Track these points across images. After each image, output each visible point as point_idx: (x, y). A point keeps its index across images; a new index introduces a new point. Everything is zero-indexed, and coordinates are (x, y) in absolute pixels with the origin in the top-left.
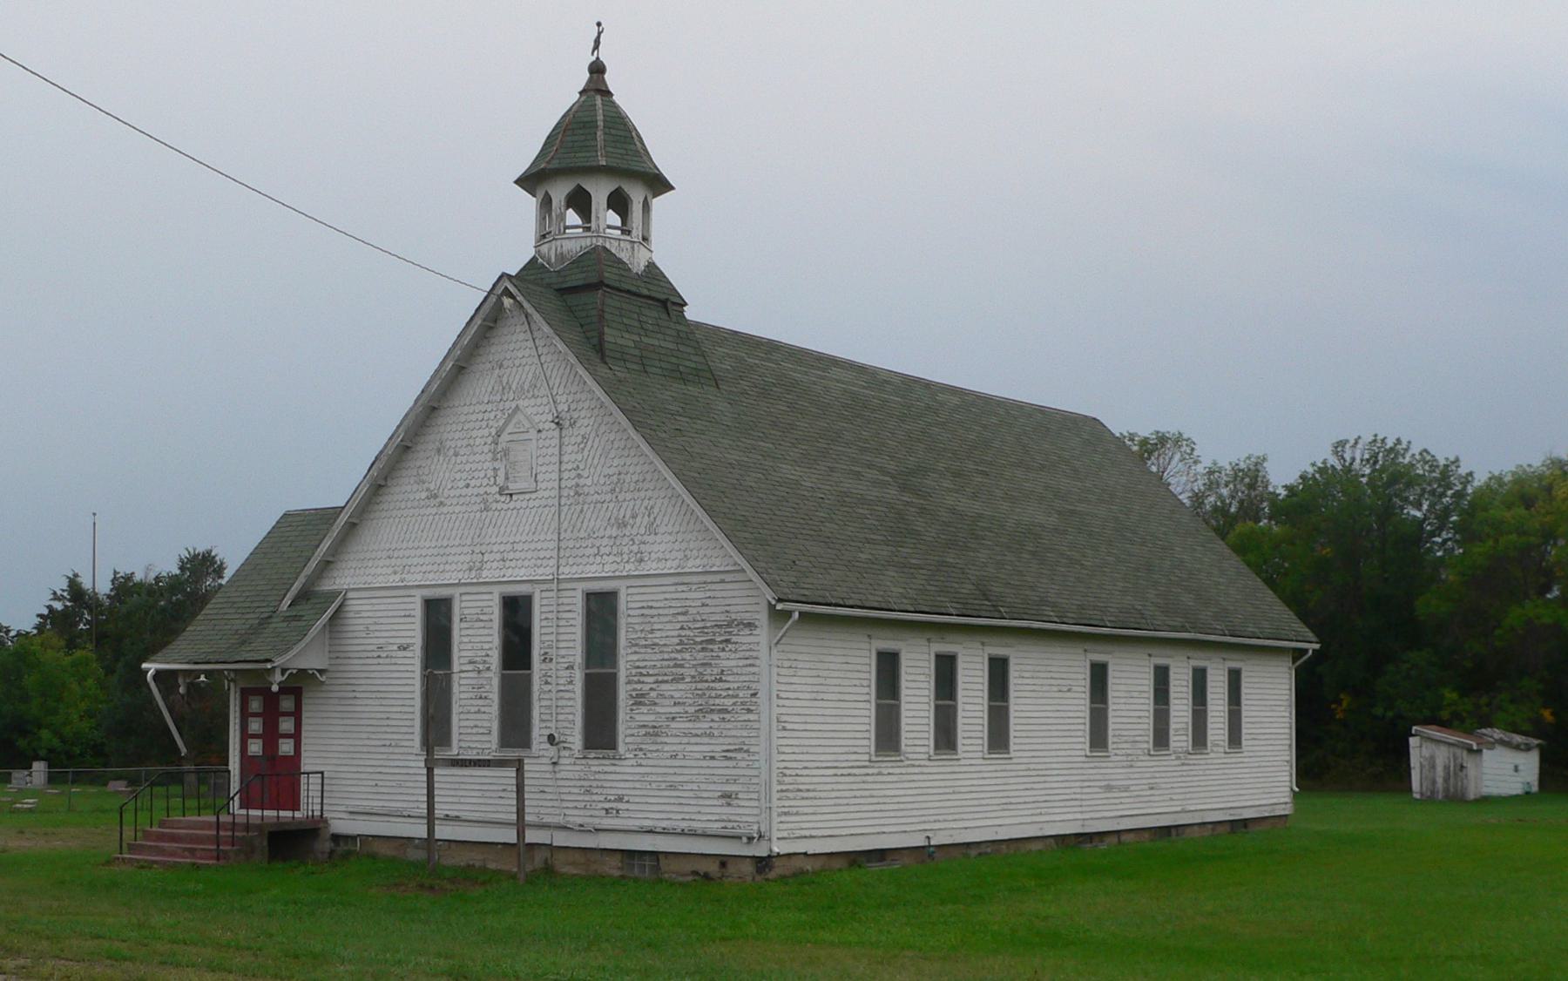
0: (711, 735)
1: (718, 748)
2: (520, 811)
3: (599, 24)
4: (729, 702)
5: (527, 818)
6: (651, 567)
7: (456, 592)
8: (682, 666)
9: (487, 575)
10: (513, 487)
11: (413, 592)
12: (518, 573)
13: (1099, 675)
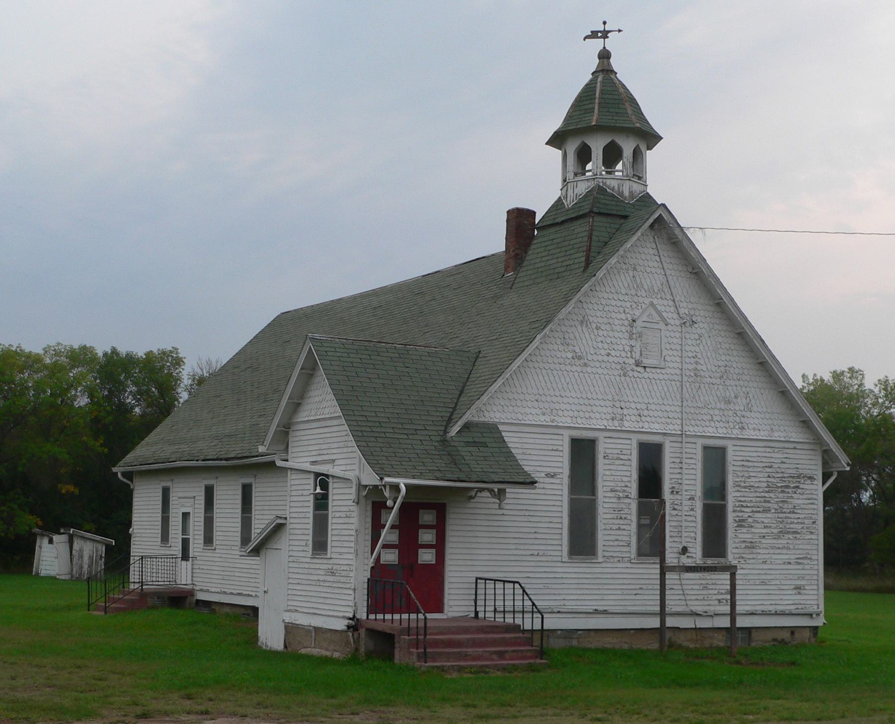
1: (793, 557)
3: (620, 31)
6: (750, 434)
8: (769, 502)
9: (628, 425)
12: (654, 426)
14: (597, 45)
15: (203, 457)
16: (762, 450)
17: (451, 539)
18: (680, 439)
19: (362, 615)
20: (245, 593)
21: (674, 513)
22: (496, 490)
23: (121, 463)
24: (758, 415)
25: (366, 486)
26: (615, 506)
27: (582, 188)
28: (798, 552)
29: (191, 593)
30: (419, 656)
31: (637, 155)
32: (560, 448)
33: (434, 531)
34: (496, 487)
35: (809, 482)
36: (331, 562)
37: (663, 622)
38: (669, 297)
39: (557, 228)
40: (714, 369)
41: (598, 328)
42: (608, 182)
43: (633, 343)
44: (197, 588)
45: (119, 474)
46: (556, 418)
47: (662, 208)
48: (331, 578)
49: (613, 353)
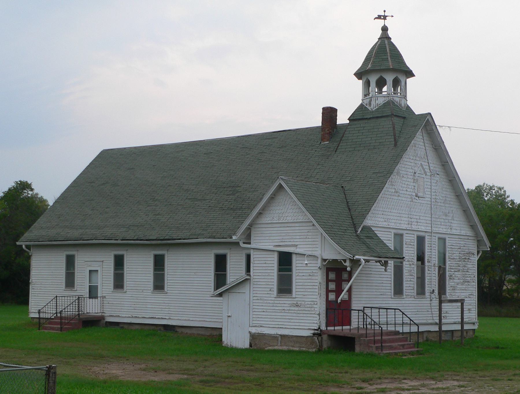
0: (466, 290)
1: (468, 294)
2: (440, 320)
3: (392, 16)
4: (469, 279)
5: (465, 320)
6: (454, 232)
7: (446, 236)
8: (459, 266)
9: (414, 227)
10: (420, 194)
11: (414, 232)
13: (70, 262)
14: (381, 23)
15: (121, 238)
16: (457, 240)
17: (33, 264)
18: (430, 234)
19: (323, 328)
20: (157, 317)
21: (429, 272)
22: (383, 262)
23: (22, 238)
24: (456, 222)
25: (326, 260)
26: (409, 269)
27: (381, 101)
28: (469, 291)
29: (103, 318)
30: (377, 348)
31: (396, 83)
32: (390, 239)
33: (335, 283)
34: (383, 260)
35: (472, 256)
36: (297, 299)
37: (440, 328)
38: (426, 161)
39: (366, 121)
40: (441, 198)
41: (403, 177)
42: (395, 98)
43: (414, 184)
44: (106, 315)
45: (24, 246)
46: (389, 223)
47: (429, 115)
48: (296, 309)
49: (408, 190)
